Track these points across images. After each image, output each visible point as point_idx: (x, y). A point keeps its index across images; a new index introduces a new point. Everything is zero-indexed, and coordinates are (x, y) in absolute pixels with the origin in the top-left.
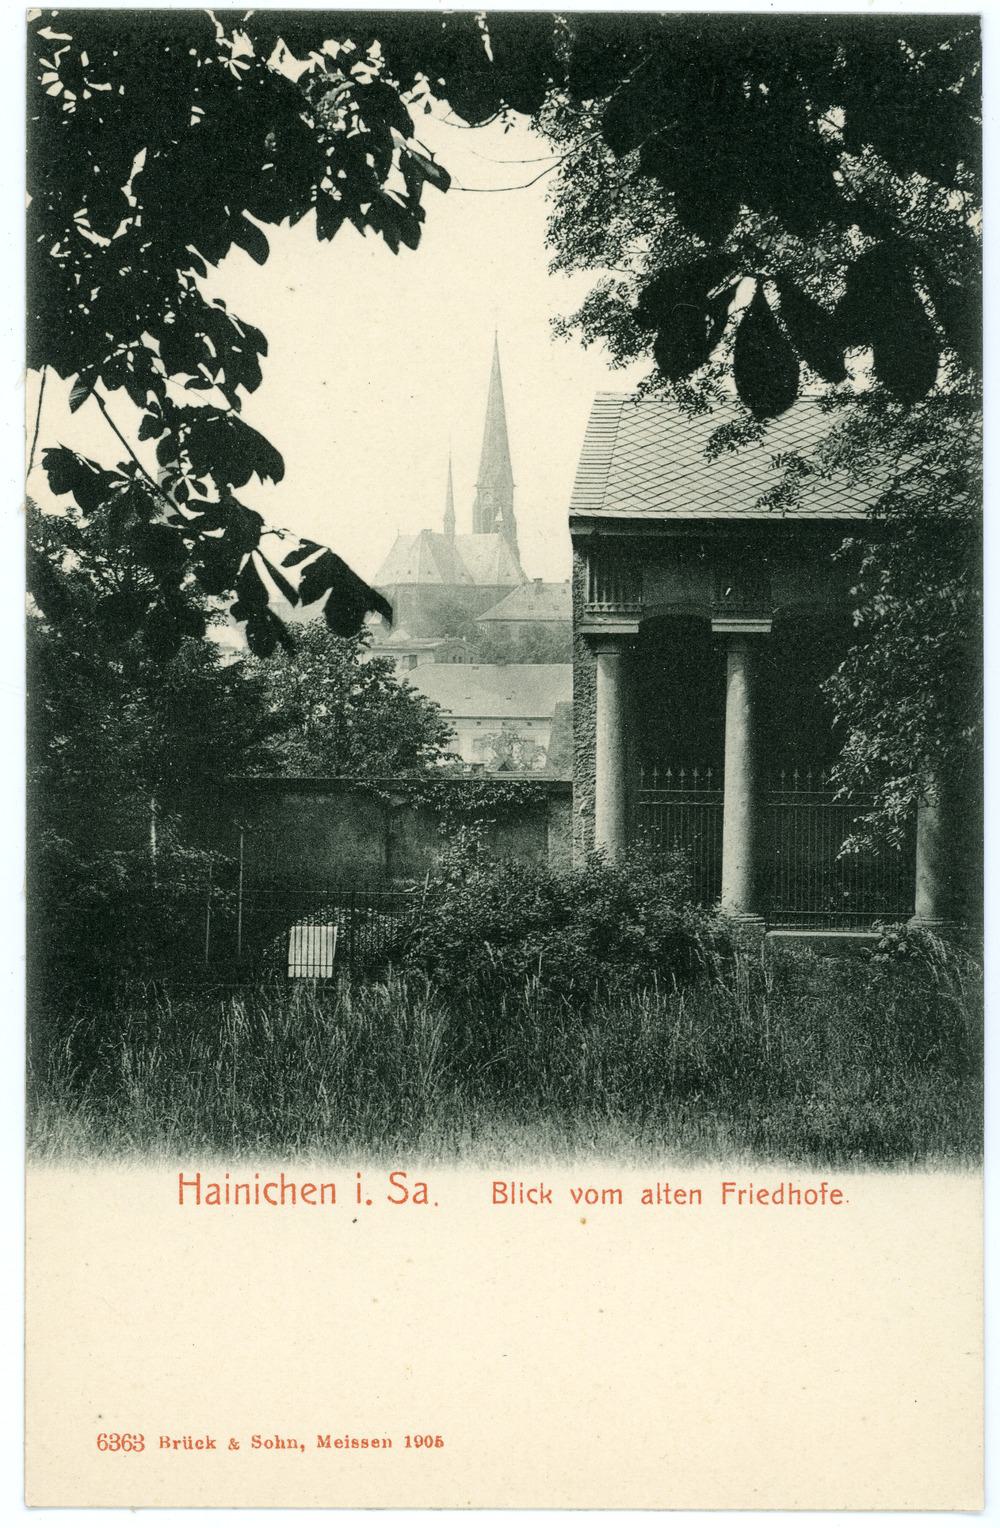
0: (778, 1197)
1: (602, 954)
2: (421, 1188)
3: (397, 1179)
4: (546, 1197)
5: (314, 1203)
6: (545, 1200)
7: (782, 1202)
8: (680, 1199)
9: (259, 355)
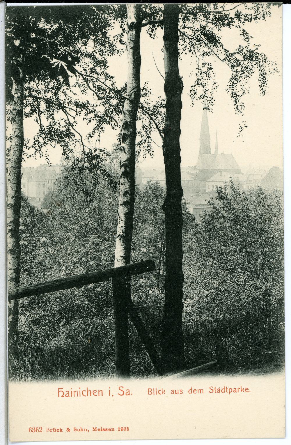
0: (223, 391)
1: (262, 252)
2: (128, 391)
3: (121, 388)
4: (164, 392)
5: (96, 396)
6: (163, 393)
7: (224, 392)
8: (195, 392)
9: (74, 66)
